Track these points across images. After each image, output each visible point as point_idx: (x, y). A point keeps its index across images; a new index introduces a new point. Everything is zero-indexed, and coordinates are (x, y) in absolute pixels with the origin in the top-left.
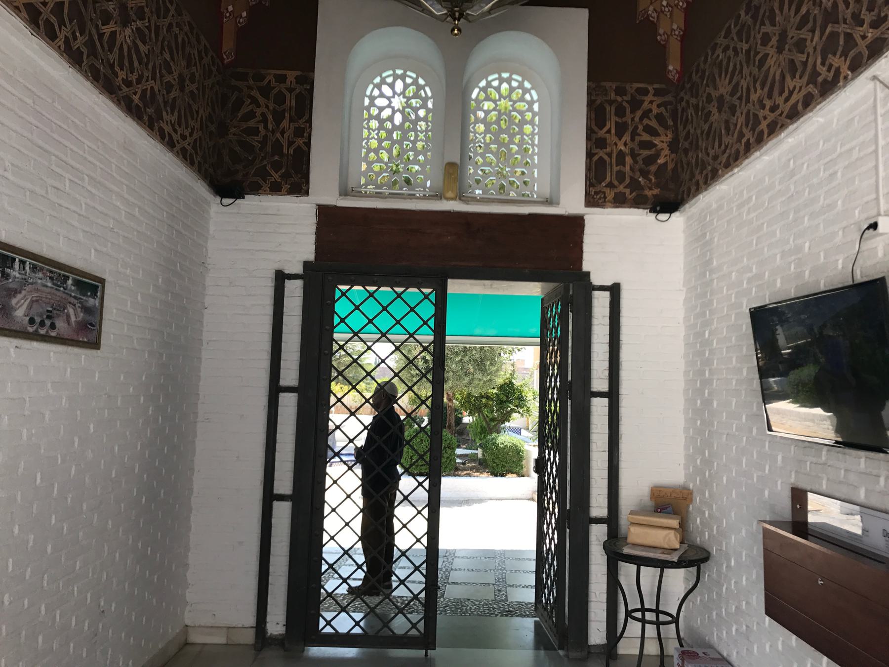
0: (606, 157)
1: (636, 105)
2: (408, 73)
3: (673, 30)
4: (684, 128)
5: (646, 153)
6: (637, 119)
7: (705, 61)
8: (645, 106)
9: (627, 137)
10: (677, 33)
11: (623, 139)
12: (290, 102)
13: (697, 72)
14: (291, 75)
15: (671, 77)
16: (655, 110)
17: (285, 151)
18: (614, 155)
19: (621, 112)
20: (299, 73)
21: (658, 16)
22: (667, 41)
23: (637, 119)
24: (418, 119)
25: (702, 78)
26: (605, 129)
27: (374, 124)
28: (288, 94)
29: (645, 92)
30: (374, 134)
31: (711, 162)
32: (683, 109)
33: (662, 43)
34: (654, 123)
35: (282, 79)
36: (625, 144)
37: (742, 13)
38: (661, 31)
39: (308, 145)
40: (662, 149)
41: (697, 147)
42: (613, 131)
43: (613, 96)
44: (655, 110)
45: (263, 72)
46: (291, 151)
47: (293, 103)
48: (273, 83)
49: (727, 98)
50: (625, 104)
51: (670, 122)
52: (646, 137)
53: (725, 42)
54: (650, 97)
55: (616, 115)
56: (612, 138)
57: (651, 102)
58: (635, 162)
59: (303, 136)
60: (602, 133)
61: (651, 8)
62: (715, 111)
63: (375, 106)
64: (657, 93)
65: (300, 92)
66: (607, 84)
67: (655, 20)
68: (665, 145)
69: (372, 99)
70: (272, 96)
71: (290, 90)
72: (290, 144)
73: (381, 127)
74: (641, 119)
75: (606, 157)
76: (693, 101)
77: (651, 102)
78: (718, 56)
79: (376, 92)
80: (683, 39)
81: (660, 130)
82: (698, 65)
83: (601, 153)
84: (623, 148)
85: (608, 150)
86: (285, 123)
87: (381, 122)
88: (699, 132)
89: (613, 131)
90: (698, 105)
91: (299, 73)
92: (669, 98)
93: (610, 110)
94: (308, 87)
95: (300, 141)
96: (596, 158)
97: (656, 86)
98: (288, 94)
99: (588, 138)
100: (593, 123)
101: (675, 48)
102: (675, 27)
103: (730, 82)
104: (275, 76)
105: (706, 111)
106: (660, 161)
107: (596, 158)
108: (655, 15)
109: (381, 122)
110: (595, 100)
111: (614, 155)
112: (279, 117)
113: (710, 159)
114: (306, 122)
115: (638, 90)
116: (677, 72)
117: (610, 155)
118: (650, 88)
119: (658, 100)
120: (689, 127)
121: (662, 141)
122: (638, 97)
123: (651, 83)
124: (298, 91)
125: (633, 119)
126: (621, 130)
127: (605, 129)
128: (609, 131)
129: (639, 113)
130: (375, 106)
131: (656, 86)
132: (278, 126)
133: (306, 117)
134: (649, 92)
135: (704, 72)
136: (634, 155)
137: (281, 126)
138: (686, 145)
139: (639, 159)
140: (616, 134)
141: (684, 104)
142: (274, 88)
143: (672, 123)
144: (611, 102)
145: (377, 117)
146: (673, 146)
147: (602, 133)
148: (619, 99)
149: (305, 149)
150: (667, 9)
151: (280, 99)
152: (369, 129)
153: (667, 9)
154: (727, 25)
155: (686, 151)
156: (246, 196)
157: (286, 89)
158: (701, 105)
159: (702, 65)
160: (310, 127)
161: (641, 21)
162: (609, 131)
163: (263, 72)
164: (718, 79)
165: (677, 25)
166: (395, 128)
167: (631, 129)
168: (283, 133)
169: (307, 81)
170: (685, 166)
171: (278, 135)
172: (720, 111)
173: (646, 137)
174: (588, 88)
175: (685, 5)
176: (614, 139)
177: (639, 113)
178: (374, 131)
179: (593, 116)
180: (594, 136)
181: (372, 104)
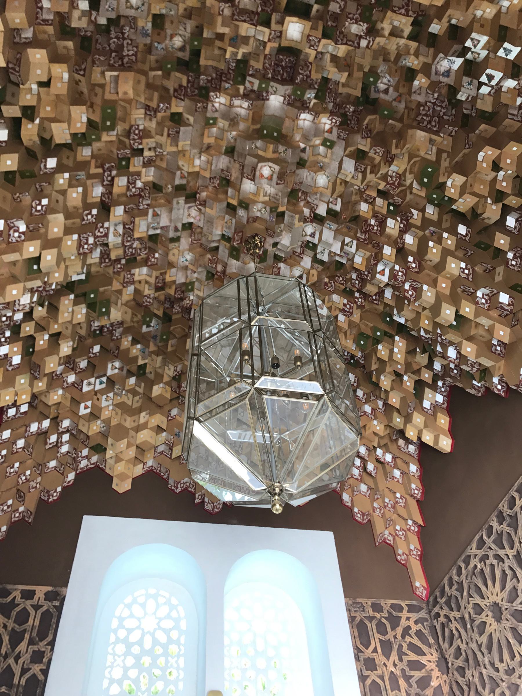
0: (379, 681)
1: (395, 622)
2: (161, 592)
3: (410, 550)
4: (451, 645)
5: (417, 675)
6: (399, 637)
7: (459, 574)
8: (403, 623)
9: (394, 656)
10: (415, 553)
11: (392, 659)
12: (34, 620)
13: (451, 585)
14: (41, 591)
15: (419, 594)
16: (414, 628)
17: (16, 681)
18: (386, 678)
19: (381, 629)
20: (50, 588)
21: (394, 539)
22: (407, 560)
23: (399, 637)
24: (170, 641)
25: (460, 589)
26: (371, 648)
27: (120, 648)
28: (32, 612)
29: (400, 609)
30: (119, 661)
31: (505, 677)
32: (442, 624)
33: (403, 562)
34: (416, 641)
35: (29, 595)
36: (395, 665)
37: (495, 524)
38: (400, 552)
39: (45, 672)
40: (432, 670)
41: (477, 663)
42: (379, 651)
43: (371, 613)
44: (414, 628)
45: (9, 587)
46: (23, 682)
47: (37, 623)
48: (18, 600)
49: (505, 605)
50: (383, 620)
51: (431, 641)
52: (413, 657)
53: (480, 553)
54: (405, 614)
55: (378, 632)
56: (380, 659)
57: (408, 619)
58: (410, 686)
59: (41, 662)
60: (368, 652)
61: (387, 532)
62: (490, 620)
63: (123, 627)
64: (412, 609)
65: (48, 610)
66: (363, 601)
67: (392, 543)
68: (433, 666)
69: (121, 620)
70: (14, 614)
71: (36, 607)
72: (24, 671)
73: (128, 653)
74: (403, 637)
75: (379, 681)
76: (455, 614)
77: (408, 619)
78: (476, 566)
79: (126, 613)
80: (423, 558)
81: (425, 648)
82: (451, 579)
83: (373, 676)
84: (393, 669)
85: (379, 672)
86: (22, 646)
87: (129, 646)
88: (474, 646)
89: (379, 651)
90: (463, 618)
91: (50, 588)
92: (423, 614)
93: (372, 627)
94: (57, 604)
95: (36, 669)
96: (368, 682)
97: (408, 602)
98: (32, 612)
99: (357, 658)
100: (358, 640)
101: (416, 567)
102: (412, 547)
103: (503, 588)
104: (23, 592)
105: (477, 623)
106: (434, 683)
107: (368, 682)
108: (390, 538)
109: (129, 646)
110: (355, 617)
111: (386, 678)
112: (16, 638)
113: (502, 674)
114: (47, 645)
115: (393, 606)
116: (425, 588)
117: (382, 678)
118: (403, 604)
119: (415, 616)
120: (457, 642)
121: (430, 659)
122: (395, 614)
123: (404, 599)
124: (45, 608)
125: (395, 637)
126: (387, 647)
127: (371, 648)
128: (375, 651)
129: (399, 631)
130: (123, 627)
131: (408, 602)
132: (13, 649)
133: (49, 638)
134: (403, 608)
135: (461, 584)
136: (407, 678)
137: (17, 650)
138: (460, 662)
139: (413, 681)
140: (383, 654)
141: (442, 619)
142: (19, 605)
143: (433, 641)
144: (371, 619)
145: (125, 641)
146: (443, 663)
147: (368, 652)
148: (377, 615)
149: (41, 677)
150: (401, 533)
151: (23, 617)
152: (114, 654)
153: (401, 533)
154: (477, 537)
155: (461, 671)
156: (411, 28)
157: (32, 606)
158: (467, 616)
159: (455, 578)
160: (52, 650)
161: (380, 543)
162: (375, 651)
163: (9, 587)
164: (483, 588)
165: (415, 545)
166: (144, 652)
167: (395, 647)
168: (17, 658)
169: (57, 598)
170: (465, 688)
171: (11, 661)
172: (499, 620)
173: (413, 657)
174: (347, 604)
175: (416, 529)
176: (383, 659)
177: (399, 631)
178: (119, 656)
179: (357, 634)
180: (362, 656)
181: (121, 626)
